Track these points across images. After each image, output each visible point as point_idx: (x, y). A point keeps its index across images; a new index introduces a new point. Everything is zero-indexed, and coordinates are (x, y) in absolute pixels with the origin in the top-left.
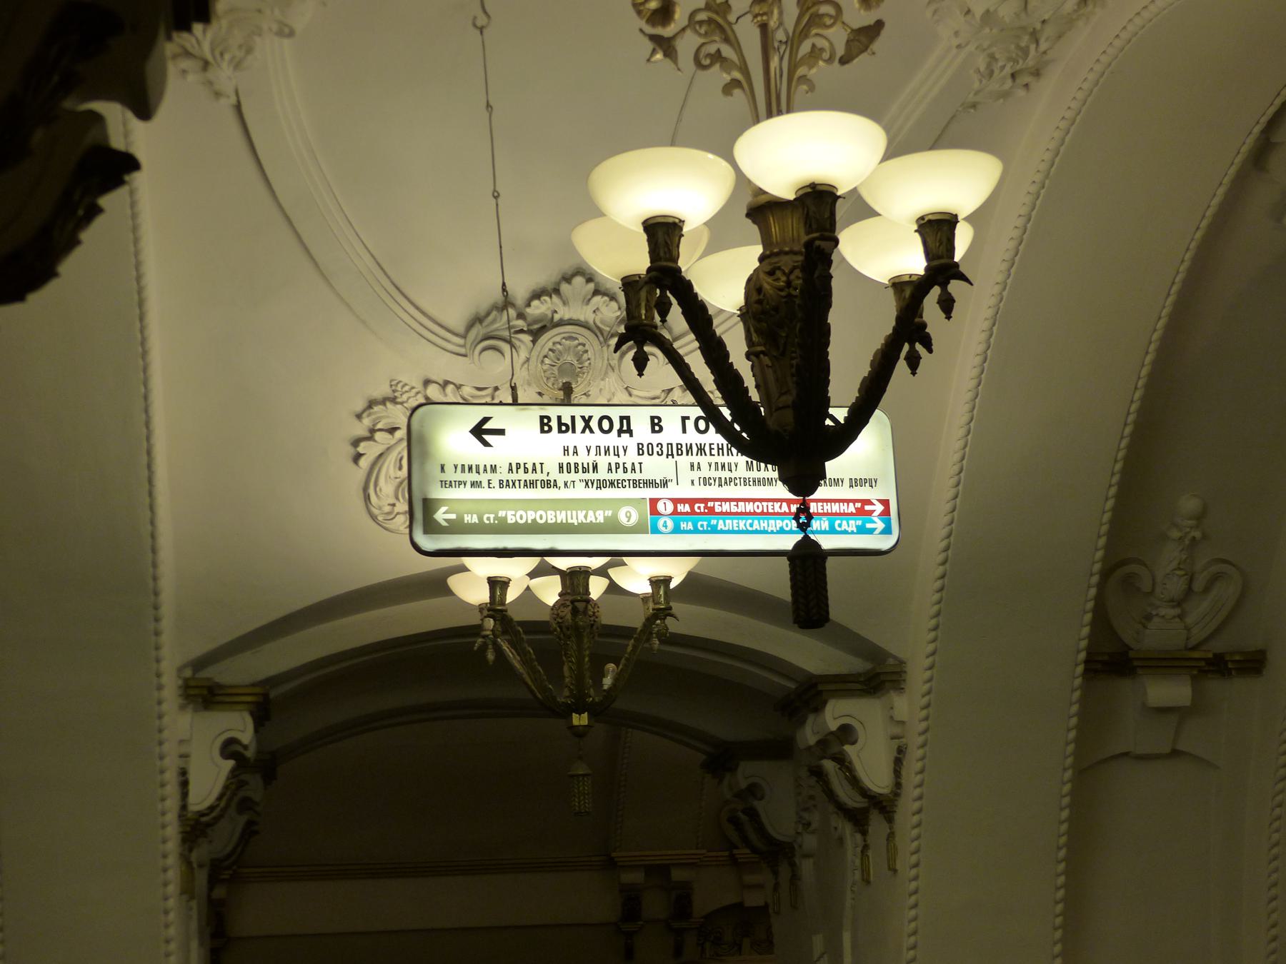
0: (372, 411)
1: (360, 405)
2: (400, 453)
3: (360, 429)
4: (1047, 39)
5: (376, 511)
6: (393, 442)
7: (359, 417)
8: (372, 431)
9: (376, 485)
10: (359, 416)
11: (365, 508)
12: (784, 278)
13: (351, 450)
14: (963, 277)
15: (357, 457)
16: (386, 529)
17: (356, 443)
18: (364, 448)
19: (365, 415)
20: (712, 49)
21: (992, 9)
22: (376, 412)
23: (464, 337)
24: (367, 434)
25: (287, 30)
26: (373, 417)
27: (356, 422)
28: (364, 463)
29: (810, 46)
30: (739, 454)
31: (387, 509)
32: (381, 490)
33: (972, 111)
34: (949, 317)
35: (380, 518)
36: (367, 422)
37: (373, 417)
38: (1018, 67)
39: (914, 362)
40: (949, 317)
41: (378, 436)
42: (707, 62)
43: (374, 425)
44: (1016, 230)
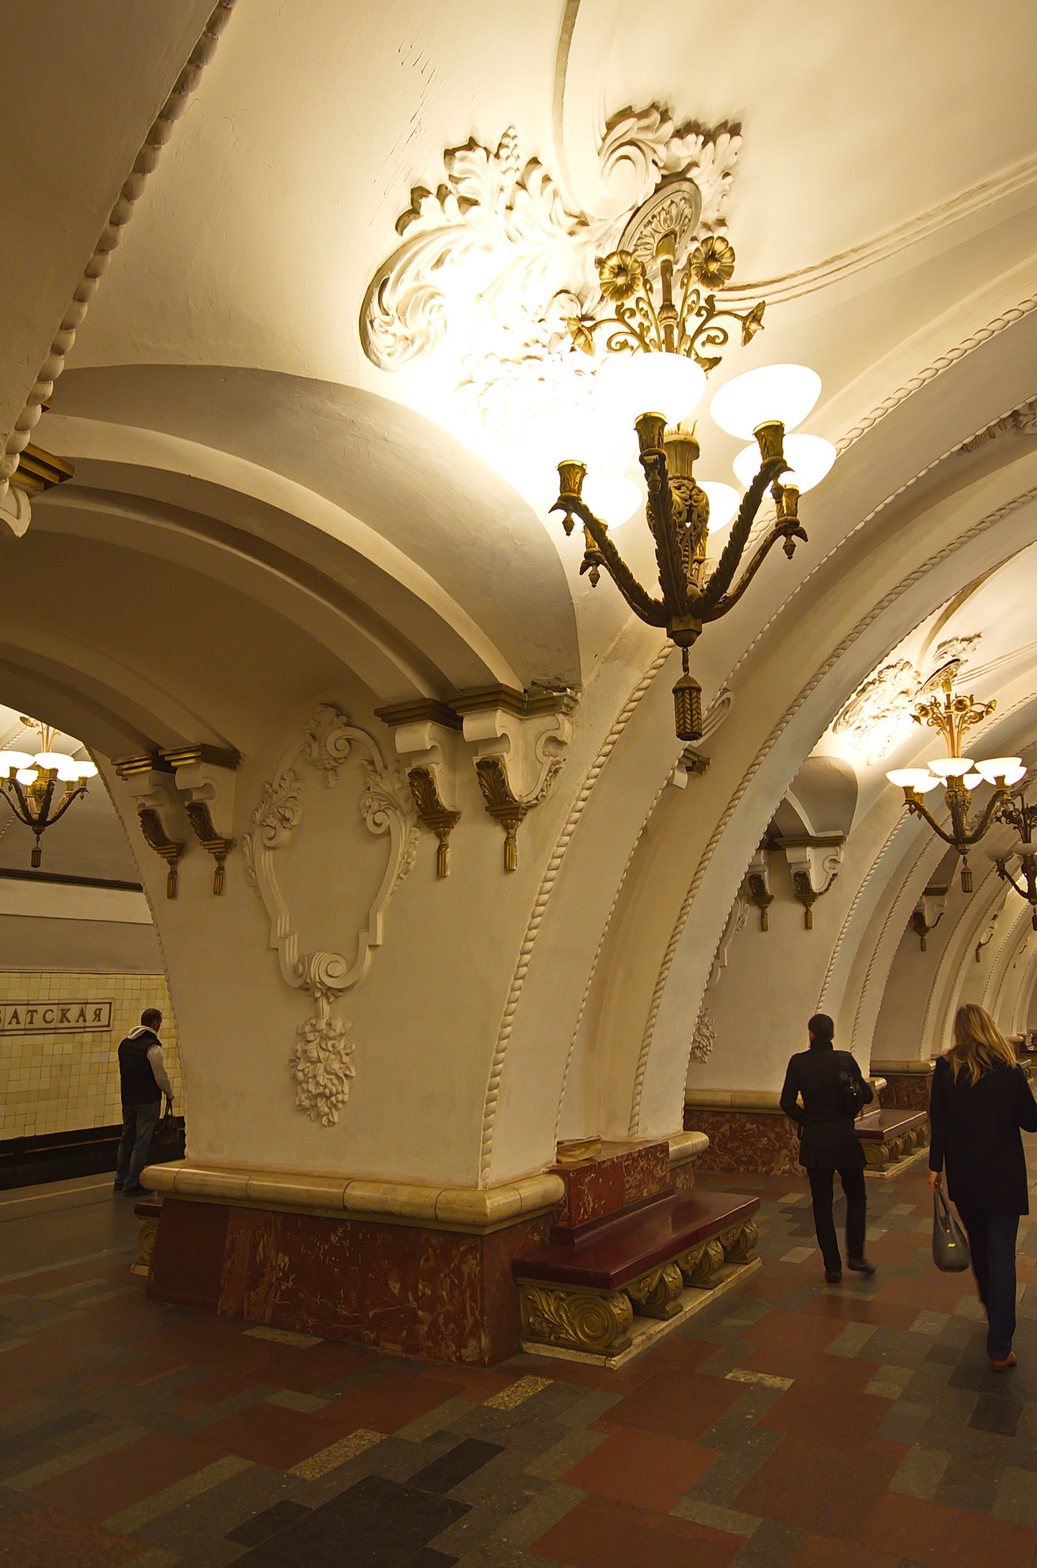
14: (87, 791)
20: (621, 338)
34: (568, 534)
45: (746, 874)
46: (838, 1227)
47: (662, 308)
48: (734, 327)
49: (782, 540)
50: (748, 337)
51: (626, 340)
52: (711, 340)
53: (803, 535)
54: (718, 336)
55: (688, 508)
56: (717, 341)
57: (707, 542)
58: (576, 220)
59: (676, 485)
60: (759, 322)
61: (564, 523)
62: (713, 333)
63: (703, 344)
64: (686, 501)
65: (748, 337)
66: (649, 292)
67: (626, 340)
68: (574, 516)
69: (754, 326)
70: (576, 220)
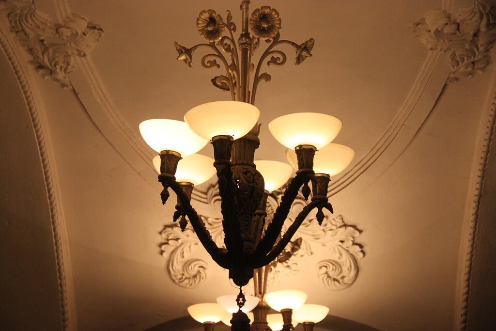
0: (166, 230)
1: (160, 228)
2: (182, 250)
3: (161, 239)
4: (481, 46)
5: (174, 278)
6: (178, 245)
7: (160, 233)
8: (168, 240)
9: (172, 265)
10: (160, 233)
11: (169, 278)
12: (252, 177)
13: (158, 249)
15: (162, 252)
16: (180, 286)
17: (161, 245)
18: (165, 248)
19: (163, 233)
20: (212, 58)
21: (439, 29)
22: (168, 231)
23: (206, 193)
24: (165, 241)
25: (82, 54)
26: (167, 233)
27: (159, 235)
28: (166, 255)
29: (271, 57)
30: (287, 261)
31: (179, 276)
32: (175, 267)
33: (456, 82)
34: (164, 203)
35: (177, 281)
36: (164, 235)
37: (167, 233)
38: (476, 59)
39: (320, 217)
40: (164, 203)
41: (170, 242)
42: (209, 65)
43: (168, 237)
44: (486, 141)
45: (232, 17)
46: (292, 150)
47: (242, 35)
48: (291, 53)
49: (315, 211)
50: (299, 60)
51: (215, 60)
52: (274, 61)
53: (330, 208)
54: (280, 60)
55: (251, 188)
56: (278, 62)
57: (270, 275)
58: (219, 235)
59: (245, 171)
60: (309, 52)
61: (162, 194)
62: (276, 55)
63: (268, 63)
64: (250, 183)
65: (299, 60)
66: (232, 32)
67: (215, 60)
68: (170, 189)
69: (304, 53)
70: (219, 235)
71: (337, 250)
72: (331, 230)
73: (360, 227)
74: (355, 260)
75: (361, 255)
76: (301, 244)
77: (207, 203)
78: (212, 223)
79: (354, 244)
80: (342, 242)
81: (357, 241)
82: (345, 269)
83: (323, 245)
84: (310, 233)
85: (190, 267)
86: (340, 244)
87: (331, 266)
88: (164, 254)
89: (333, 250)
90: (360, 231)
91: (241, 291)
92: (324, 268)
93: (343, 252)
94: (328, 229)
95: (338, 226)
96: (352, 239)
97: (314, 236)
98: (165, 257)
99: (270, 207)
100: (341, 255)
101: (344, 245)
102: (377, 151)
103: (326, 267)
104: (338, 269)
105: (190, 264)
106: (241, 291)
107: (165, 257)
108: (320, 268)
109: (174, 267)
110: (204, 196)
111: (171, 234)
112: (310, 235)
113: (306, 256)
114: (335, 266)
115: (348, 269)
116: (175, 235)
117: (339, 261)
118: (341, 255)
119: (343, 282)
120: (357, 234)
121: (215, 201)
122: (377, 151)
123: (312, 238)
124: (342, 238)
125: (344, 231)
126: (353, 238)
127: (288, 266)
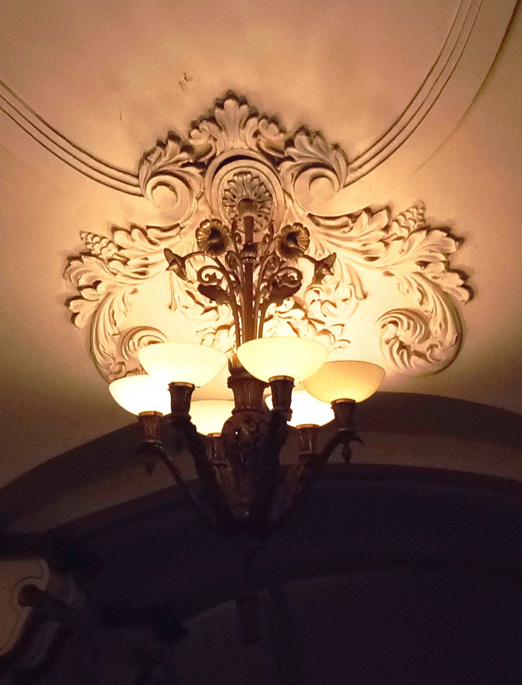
2: (110, 307)
5: (104, 370)
65: (318, 278)
71: (415, 285)
72: (399, 238)
73: (459, 230)
74: (457, 312)
75: (465, 294)
76: (332, 265)
77: (141, 195)
78: (155, 240)
79: (449, 269)
80: (424, 264)
81: (456, 263)
82: (434, 327)
83: (388, 274)
84: (357, 245)
85: (131, 343)
86: (418, 269)
87: (405, 320)
88: (78, 320)
89: (406, 284)
90: (460, 240)
91: (312, 259)
92: (391, 325)
93: (428, 289)
94: (395, 237)
95: (412, 229)
96: (443, 258)
97: (364, 252)
98: (82, 327)
99: (263, 187)
100: (424, 294)
101: (428, 272)
102: (412, 132)
103: (395, 323)
104: (421, 330)
105: (131, 338)
106: (312, 259)
107: (82, 327)
108: (384, 326)
109: (101, 348)
110: (135, 181)
111: (81, 273)
112: (356, 251)
113: (354, 300)
114: (413, 320)
115: (441, 325)
116: (92, 274)
117: (422, 308)
118: (424, 294)
119: (431, 355)
120: (453, 246)
121: (154, 188)
122: (412, 132)
123: (360, 258)
124: (424, 254)
125: (426, 239)
126: (447, 255)
127: (325, 332)
